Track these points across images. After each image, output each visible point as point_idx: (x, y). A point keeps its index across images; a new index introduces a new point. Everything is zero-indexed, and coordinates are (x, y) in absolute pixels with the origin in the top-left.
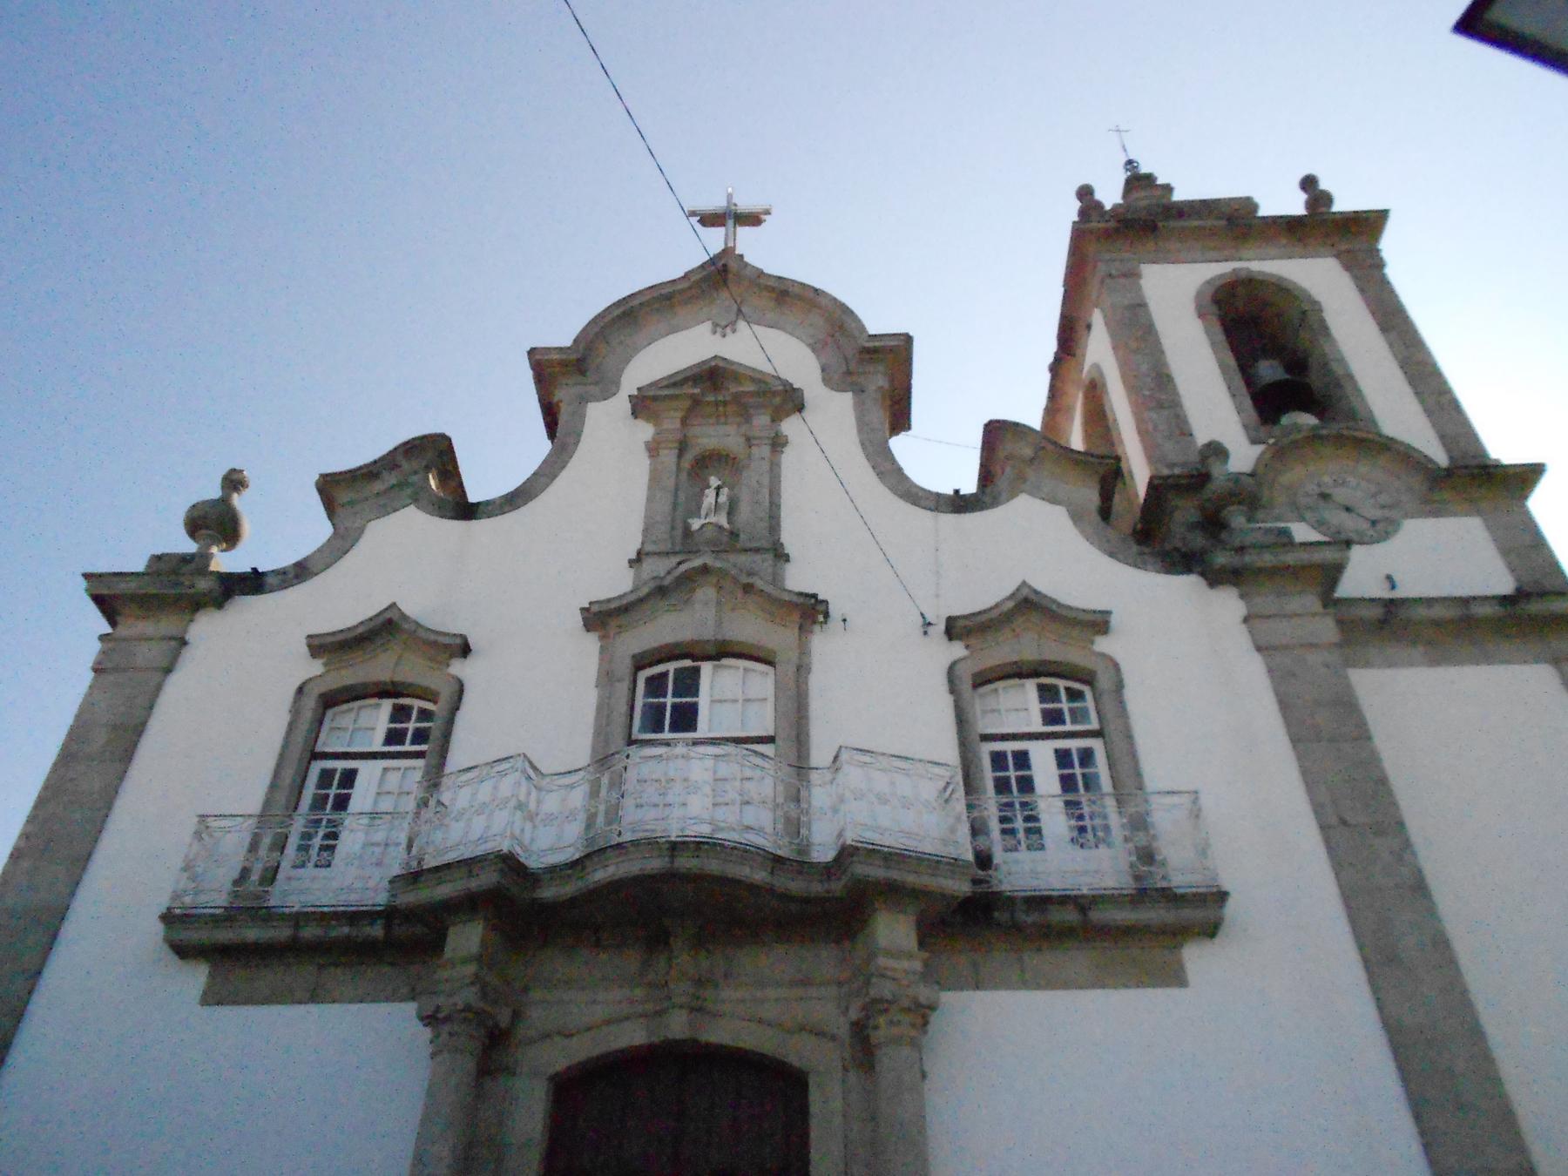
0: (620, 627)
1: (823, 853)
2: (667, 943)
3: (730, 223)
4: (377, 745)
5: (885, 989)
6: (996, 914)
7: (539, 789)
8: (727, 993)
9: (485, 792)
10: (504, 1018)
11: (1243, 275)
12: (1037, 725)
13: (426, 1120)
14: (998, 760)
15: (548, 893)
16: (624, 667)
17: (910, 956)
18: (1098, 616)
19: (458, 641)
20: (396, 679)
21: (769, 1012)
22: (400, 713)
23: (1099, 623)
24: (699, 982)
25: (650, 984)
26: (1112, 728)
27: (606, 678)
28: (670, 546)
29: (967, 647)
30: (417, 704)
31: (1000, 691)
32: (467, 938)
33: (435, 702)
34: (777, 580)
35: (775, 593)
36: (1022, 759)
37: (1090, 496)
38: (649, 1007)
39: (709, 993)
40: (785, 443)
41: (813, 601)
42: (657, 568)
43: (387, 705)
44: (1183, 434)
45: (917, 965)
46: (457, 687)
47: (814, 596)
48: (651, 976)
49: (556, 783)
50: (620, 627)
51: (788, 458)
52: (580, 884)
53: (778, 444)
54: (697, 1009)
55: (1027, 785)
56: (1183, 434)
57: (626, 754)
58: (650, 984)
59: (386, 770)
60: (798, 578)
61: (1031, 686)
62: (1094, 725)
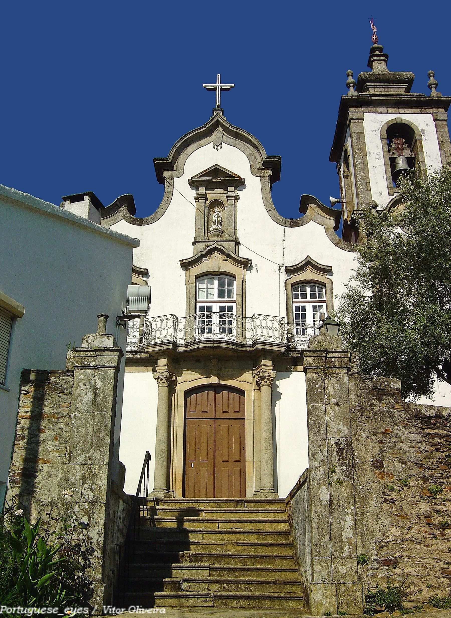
1: (249, 341)
3: (267, 363)
11: (399, 121)
14: (297, 308)
15: (179, 349)
16: (193, 279)
23: (328, 271)
26: (329, 301)
27: (188, 282)
32: (163, 362)
34: (236, 252)
35: (236, 257)
36: (304, 308)
37: (332, 223)
40: (239, 198)
41: (247, 260)
42: (201, 246)
44: (367, 190)
45: (272, 368)
47: (248, 259)
51: (240, 203)
53: (237, 198)
55: (304, 316)
56: (367, 190)
60: (243, 253)
62: (324, 299)
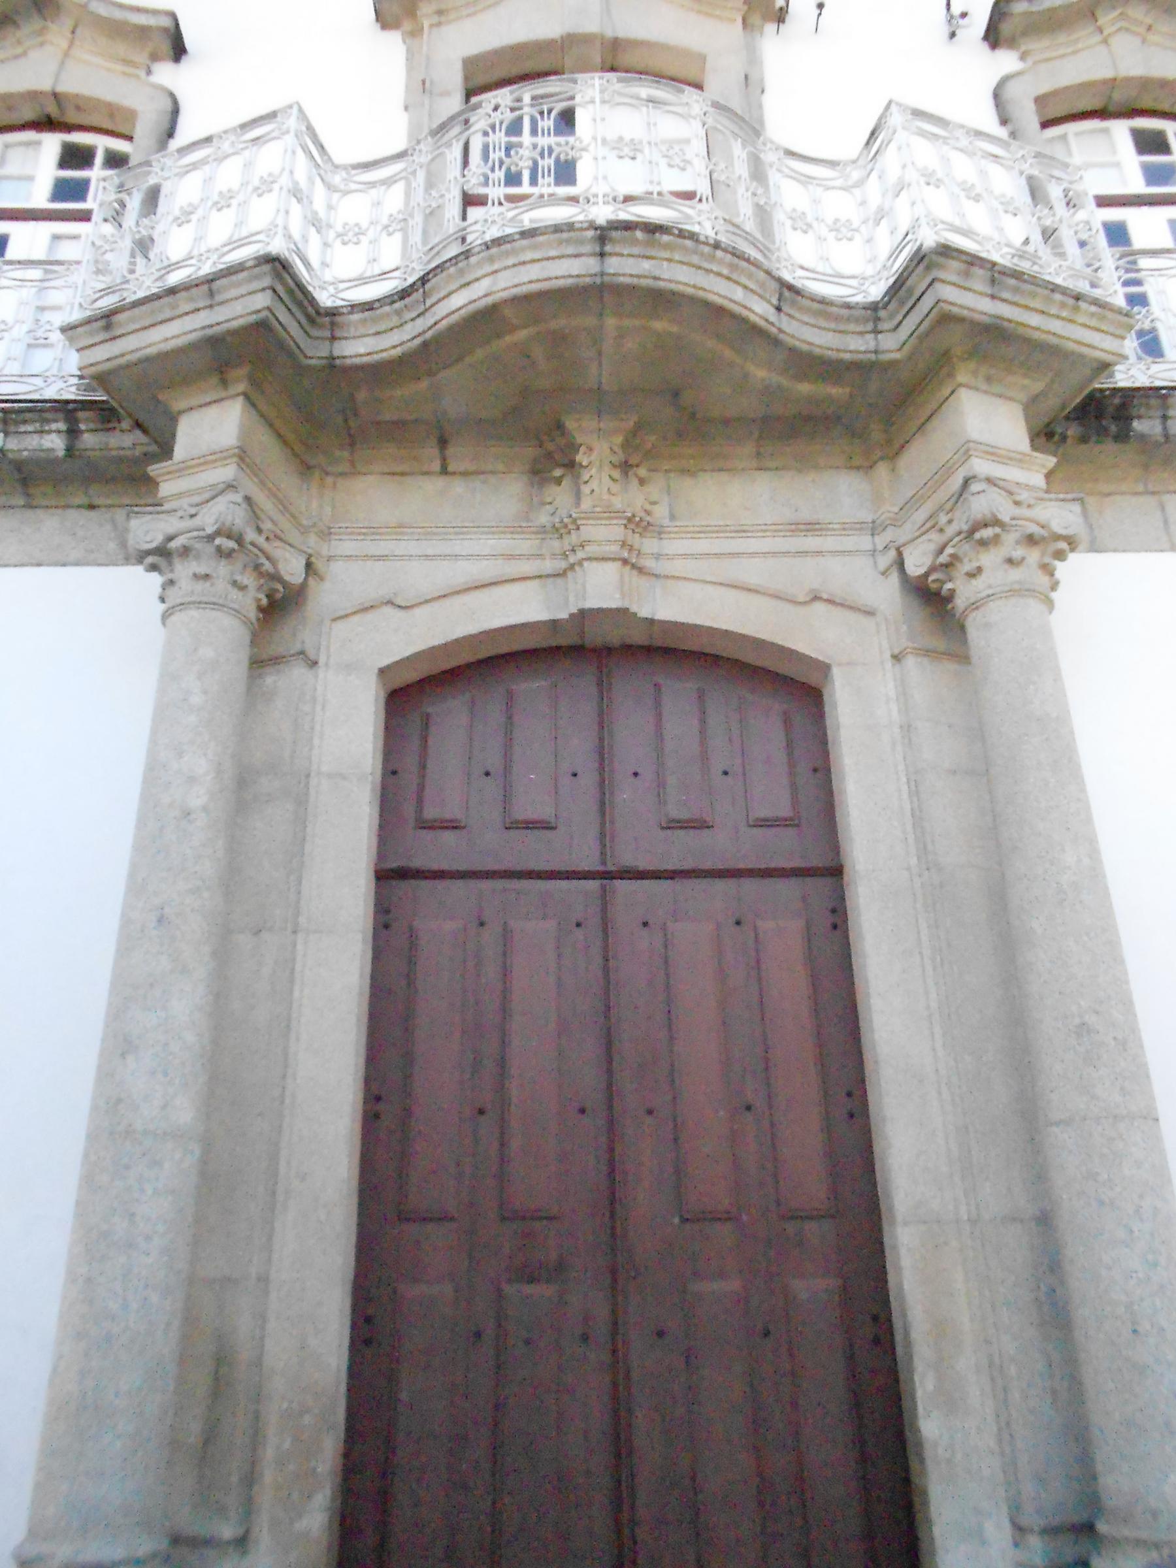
0: (440, 12)
2: (571, 465)
4: (39, 197)
5: (982, 504)
6: (1136, 424)
7: (330, 187)
8: (673, 546)
9: (229, 174)
10: (292, 569)
12: (1137, 185)
13: (162, 715)
17: (1018, 460)
18: (934, 405)
19: (166, 22)
20: (61, 88)
21: (752, 572)
22: (75, 157)
24: (639, 524)
25: (542, 530)
28: (324, 769)
29: (1023, 58)
30: (102, 143)
31: (1072, 139)
33: (130, 138)
38: (549, 566)
39: (649, 545)
43: (52, 144)
46: (167, 105)
48: (543, 518)
49: (357, 178)
50: (440, 12)
52: (421, 324)
54: (631, 563)
57: (492, 106)
58: (542, 530)
59: (56, 237)
61: (1121, 131)
